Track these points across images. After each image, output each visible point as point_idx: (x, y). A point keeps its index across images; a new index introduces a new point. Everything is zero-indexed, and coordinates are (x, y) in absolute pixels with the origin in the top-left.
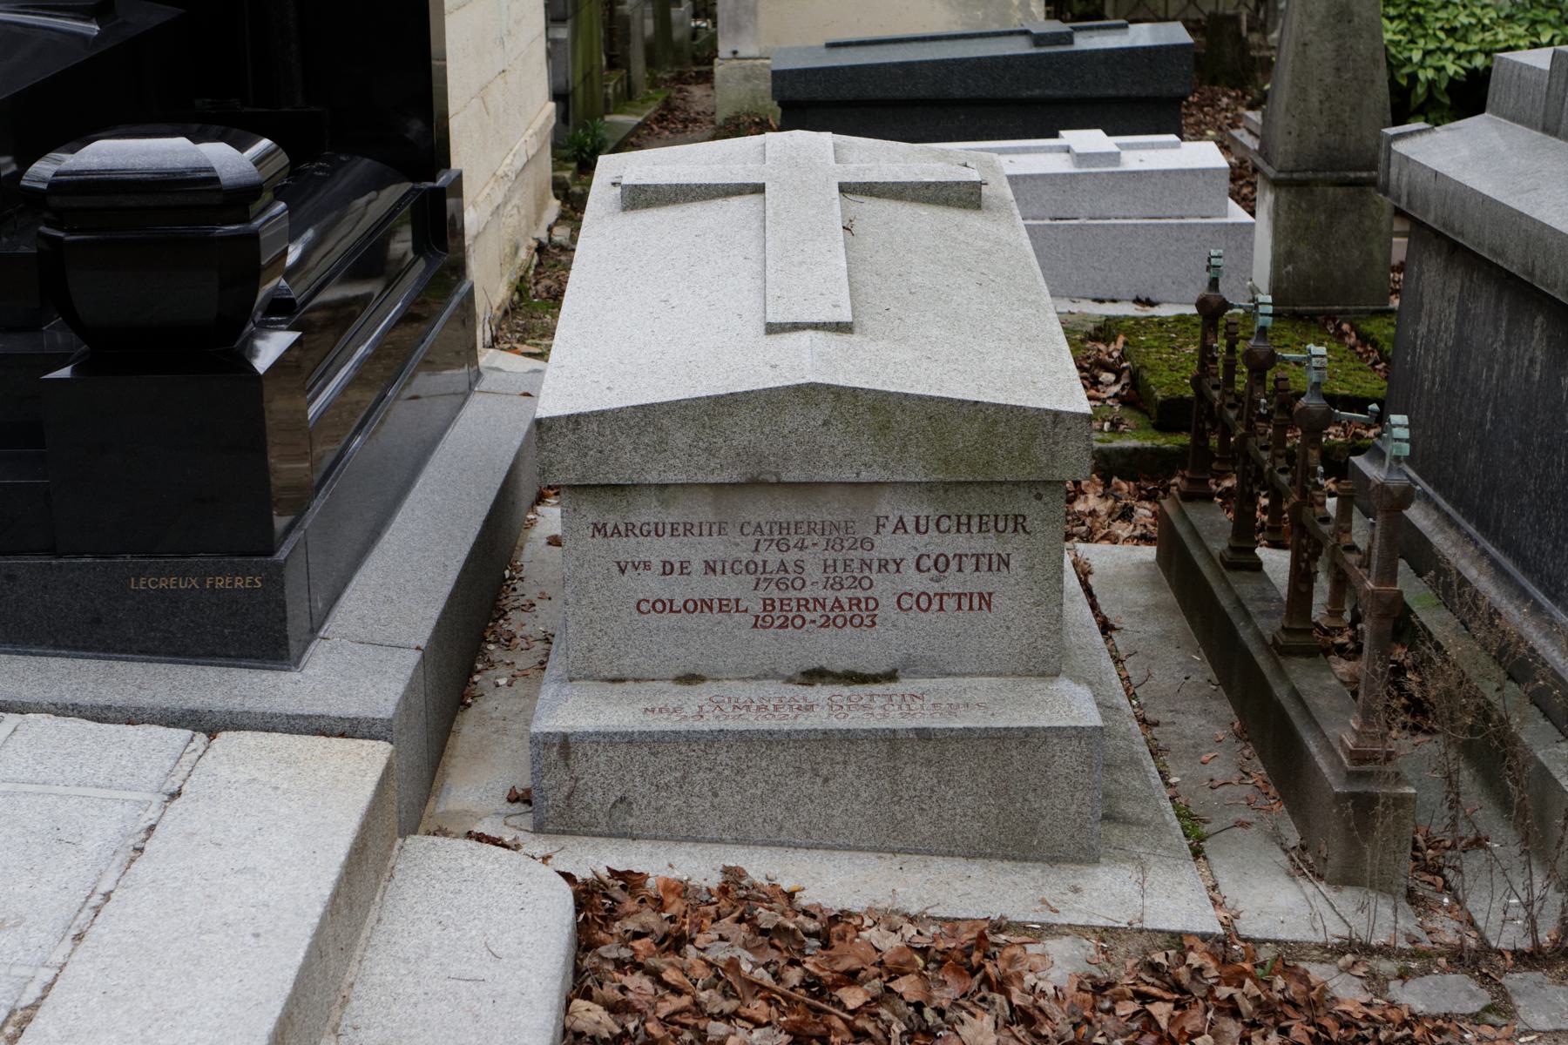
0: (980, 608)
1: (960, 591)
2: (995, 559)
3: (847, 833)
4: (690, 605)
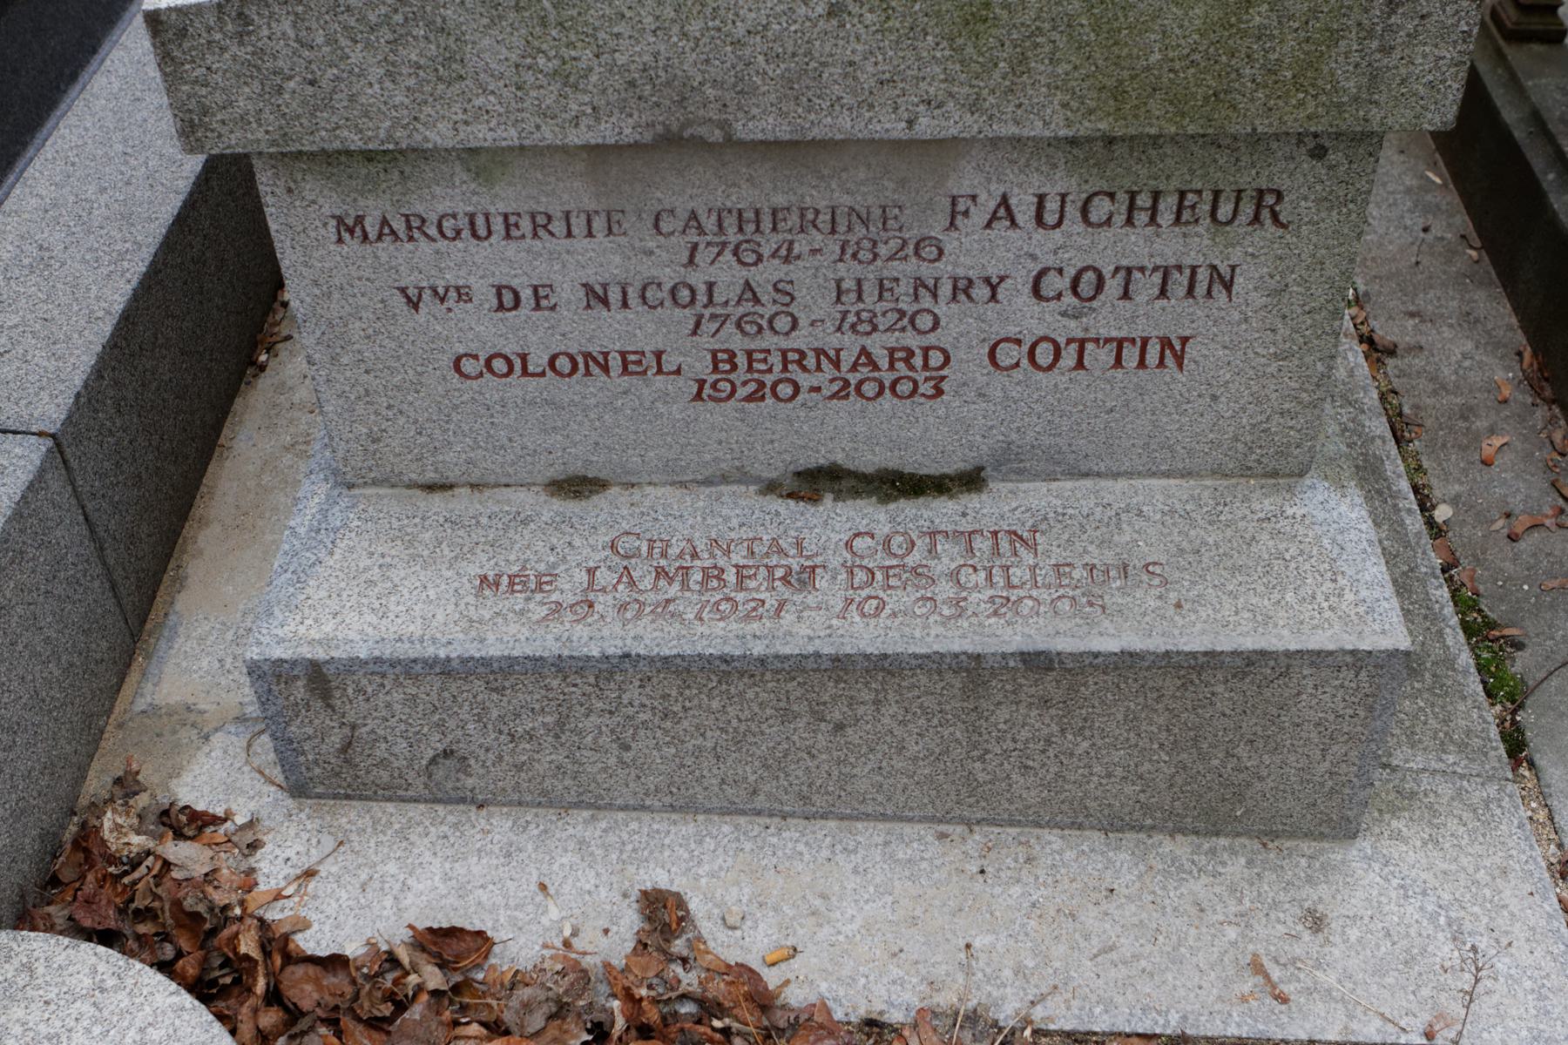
0: (1161, 364)
1: (1123, 334)
2: (1203, 275)
3: (880, 798)
4: (563, 364)
